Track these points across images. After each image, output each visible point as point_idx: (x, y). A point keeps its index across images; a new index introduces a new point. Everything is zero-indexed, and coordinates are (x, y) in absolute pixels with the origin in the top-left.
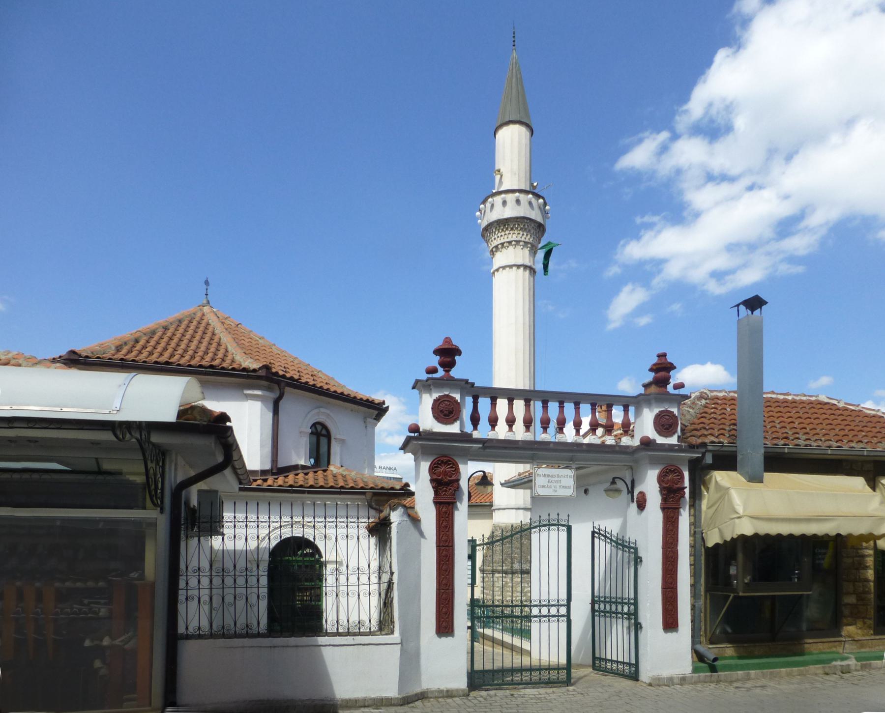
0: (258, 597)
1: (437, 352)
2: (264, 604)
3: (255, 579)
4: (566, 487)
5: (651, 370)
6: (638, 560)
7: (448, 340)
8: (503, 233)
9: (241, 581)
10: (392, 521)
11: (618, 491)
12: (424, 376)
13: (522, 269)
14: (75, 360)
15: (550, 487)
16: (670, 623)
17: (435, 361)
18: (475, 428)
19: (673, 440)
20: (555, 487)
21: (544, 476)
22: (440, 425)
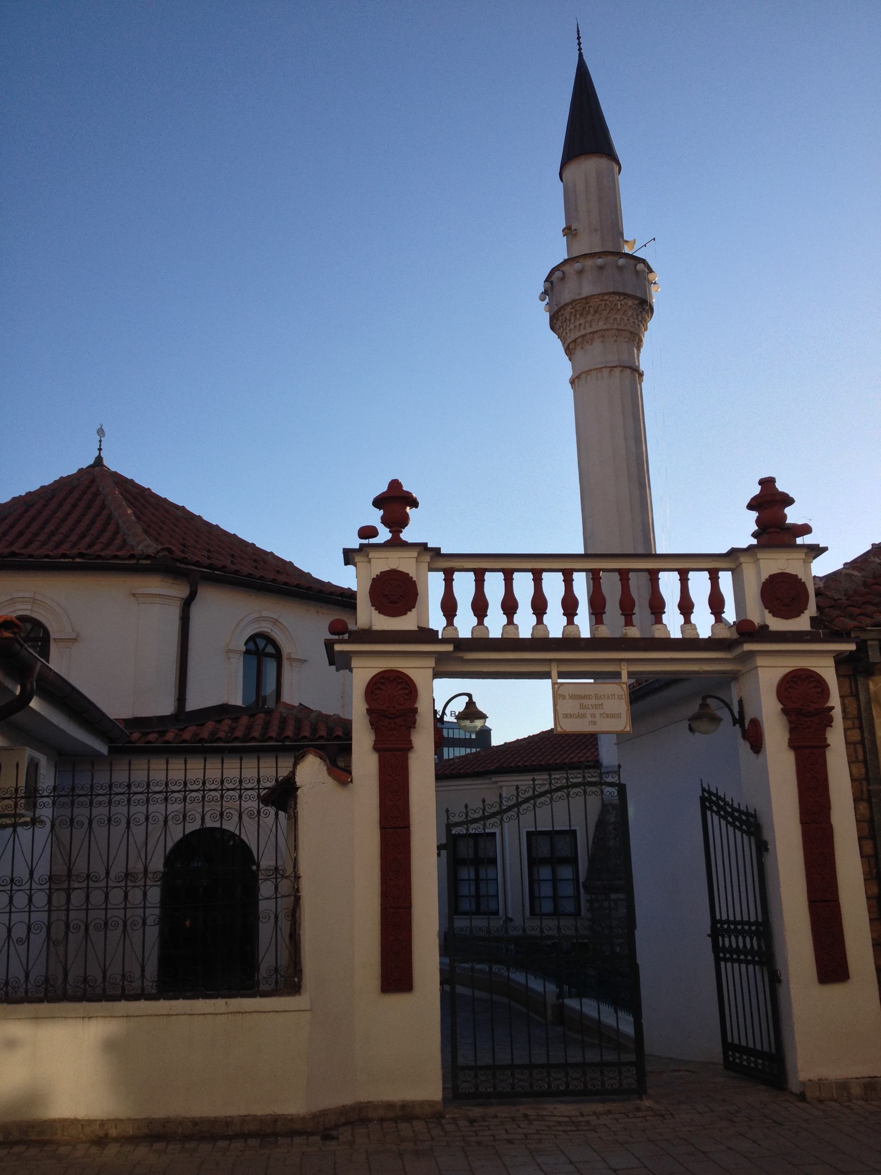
0: (67, 926)
1: (378, 502)
2: (153, 932)
3: (139, 893)
4: (612, 716)
5: (751, 506)
6: (762, 847)
7: (395, 485)
8: (582, 321)
9: (116, 896)
10: (298, 784)
11: (716, 720)
12: (355, 542)
13: (606, 372)
15: (584, 716)
16: (832, 967)
17: (374, 517)
18: (629, 623)
19: (802, 623)
21: (573, 697)
22: (382, 617)
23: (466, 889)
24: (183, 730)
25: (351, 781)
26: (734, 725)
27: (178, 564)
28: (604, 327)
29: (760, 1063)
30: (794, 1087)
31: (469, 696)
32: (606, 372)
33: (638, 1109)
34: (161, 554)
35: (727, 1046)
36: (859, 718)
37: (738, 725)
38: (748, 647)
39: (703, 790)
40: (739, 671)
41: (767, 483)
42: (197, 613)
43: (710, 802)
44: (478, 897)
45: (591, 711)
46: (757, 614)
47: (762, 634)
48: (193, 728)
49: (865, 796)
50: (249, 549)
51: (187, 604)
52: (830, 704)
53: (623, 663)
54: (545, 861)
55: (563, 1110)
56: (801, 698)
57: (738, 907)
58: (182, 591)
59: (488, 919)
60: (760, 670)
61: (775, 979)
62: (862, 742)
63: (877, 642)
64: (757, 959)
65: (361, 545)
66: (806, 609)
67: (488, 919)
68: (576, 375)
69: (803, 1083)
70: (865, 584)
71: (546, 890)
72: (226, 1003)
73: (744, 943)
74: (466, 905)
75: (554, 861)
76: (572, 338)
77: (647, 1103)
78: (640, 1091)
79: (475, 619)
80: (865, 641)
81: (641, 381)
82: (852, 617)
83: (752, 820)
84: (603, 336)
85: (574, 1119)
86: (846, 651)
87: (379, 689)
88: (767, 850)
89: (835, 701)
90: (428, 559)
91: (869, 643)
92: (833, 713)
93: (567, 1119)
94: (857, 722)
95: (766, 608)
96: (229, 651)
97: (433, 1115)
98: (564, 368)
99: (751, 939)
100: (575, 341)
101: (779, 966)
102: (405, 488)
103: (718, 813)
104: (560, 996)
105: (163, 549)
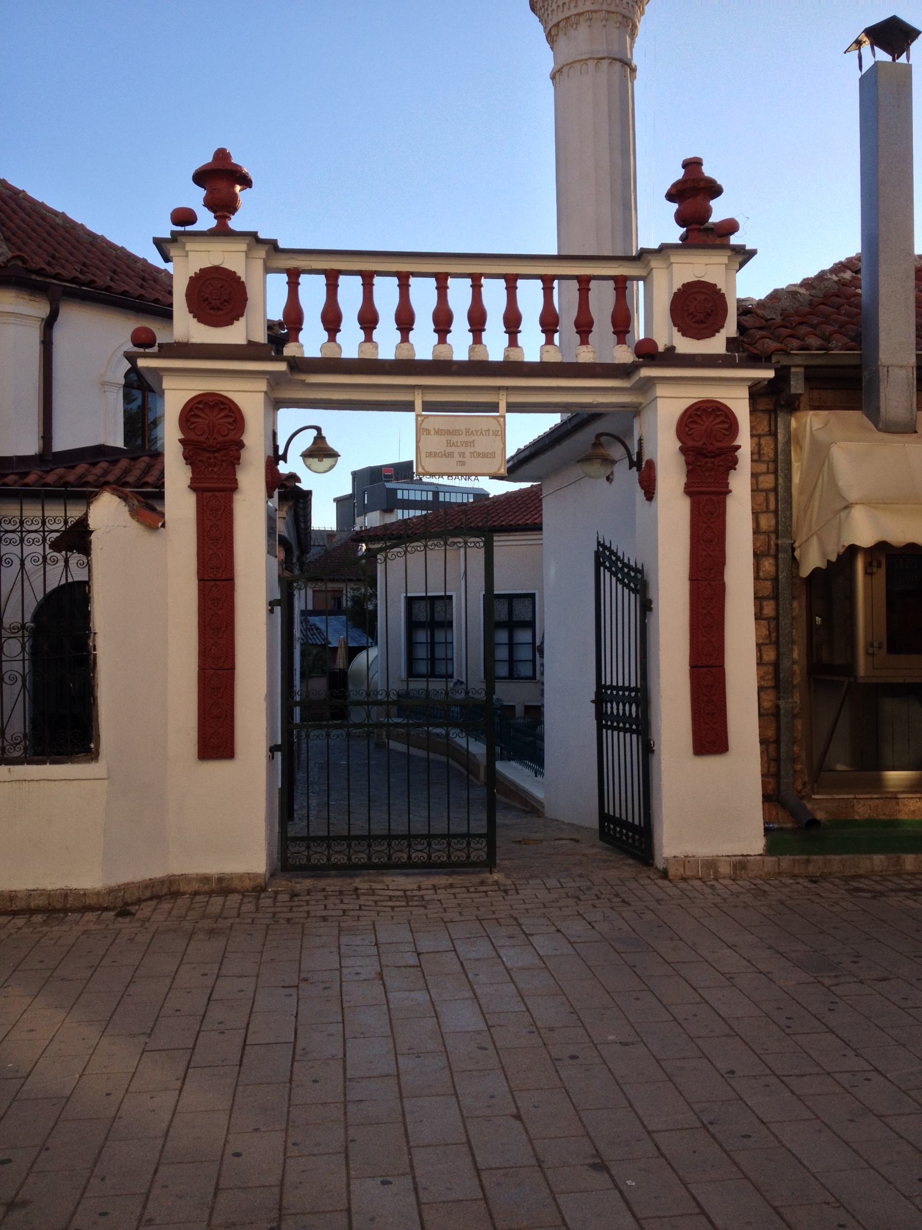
1: (200, 178)
4: (485, 455)
5: (670, 197)
6: (646, 606)
7: (222, 155)
10: (92, 527)
13: (591, 64)
14: (284, 987)
15: (450, 455)
16: (710, 736)
17: (194, 198)
19: (716, 345)
20: (462, 455)
21: (438, 432)
22: (203, 328)
23: (422, 652)
24: (47, 472)
25: (163, 526)
26: (630, 469)
27: (34, 277)
28: (592, 8)
29: (629, 835)
30: (660, 864)
31: (318, 429)
32: (591, 64)
33: (482, 883)
34: (12, 263)
35: (603, 816)
36: (775, 461)
37: (635, 469)
38: (645, 372)
39: (599, 543)
40: (641, 404)
41: (692, 165)
42: (60, 335)
43: (605, 558)
44: (432, 660)
45: (461, 449)
46: (665, 335)
47: (670, 358)
48: (60, 471)
49: (772, 552)
50: (139, 265)
51: (49, 324)
52: (736, 443)
53: (501, 392)
54: (500, 625)
55: (400, 882)
56: (705, 435)
57: (621, 674)
58: (42, 310)
59: (428, 681)
60: (660, 402)
61: (648, 749)
62: (775, 489)
63: (802, 370)
64: (634, 727)
65: (173, 233)
66: (722, 327)
67: (428, 681)
68: (557, 68)
69: (667, 860)
70: (811, 304)
71: (502, 653)
72: (9, 771)
73: (624, 710)
74: (422, 668)
75: (512, 625)
76: (555, 21)
77: (496, 876)
78: (490, 864)
79: (326, 334)
80: (788, 368)
81: (633, 78)
82: (778, 339)
83: (639, 576)
84: (590, 19)
85: (409, 893)
86: (764, 379)
87: (196, 416)
88: (651, 609)
89: (744, 441)
90: (263, 254)
91: (793, 370)
92: (739, 453)
93: (401, 893)
94: (771, 466)
95: (675, 326)
96: (104, 384)
97: (257, 889)
98: (545, 59)
99: (618, 706)
100: (557, 25)
101: (654, 736)
102: (235, 160)
103: (609, 569)
104: (491, 758)
105: (13, 258)
